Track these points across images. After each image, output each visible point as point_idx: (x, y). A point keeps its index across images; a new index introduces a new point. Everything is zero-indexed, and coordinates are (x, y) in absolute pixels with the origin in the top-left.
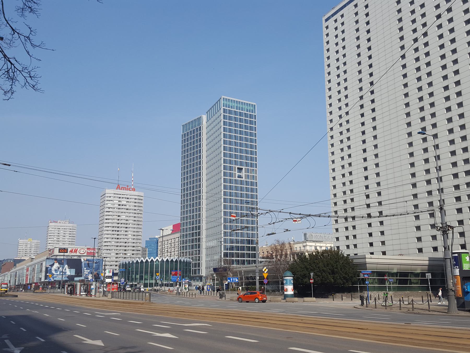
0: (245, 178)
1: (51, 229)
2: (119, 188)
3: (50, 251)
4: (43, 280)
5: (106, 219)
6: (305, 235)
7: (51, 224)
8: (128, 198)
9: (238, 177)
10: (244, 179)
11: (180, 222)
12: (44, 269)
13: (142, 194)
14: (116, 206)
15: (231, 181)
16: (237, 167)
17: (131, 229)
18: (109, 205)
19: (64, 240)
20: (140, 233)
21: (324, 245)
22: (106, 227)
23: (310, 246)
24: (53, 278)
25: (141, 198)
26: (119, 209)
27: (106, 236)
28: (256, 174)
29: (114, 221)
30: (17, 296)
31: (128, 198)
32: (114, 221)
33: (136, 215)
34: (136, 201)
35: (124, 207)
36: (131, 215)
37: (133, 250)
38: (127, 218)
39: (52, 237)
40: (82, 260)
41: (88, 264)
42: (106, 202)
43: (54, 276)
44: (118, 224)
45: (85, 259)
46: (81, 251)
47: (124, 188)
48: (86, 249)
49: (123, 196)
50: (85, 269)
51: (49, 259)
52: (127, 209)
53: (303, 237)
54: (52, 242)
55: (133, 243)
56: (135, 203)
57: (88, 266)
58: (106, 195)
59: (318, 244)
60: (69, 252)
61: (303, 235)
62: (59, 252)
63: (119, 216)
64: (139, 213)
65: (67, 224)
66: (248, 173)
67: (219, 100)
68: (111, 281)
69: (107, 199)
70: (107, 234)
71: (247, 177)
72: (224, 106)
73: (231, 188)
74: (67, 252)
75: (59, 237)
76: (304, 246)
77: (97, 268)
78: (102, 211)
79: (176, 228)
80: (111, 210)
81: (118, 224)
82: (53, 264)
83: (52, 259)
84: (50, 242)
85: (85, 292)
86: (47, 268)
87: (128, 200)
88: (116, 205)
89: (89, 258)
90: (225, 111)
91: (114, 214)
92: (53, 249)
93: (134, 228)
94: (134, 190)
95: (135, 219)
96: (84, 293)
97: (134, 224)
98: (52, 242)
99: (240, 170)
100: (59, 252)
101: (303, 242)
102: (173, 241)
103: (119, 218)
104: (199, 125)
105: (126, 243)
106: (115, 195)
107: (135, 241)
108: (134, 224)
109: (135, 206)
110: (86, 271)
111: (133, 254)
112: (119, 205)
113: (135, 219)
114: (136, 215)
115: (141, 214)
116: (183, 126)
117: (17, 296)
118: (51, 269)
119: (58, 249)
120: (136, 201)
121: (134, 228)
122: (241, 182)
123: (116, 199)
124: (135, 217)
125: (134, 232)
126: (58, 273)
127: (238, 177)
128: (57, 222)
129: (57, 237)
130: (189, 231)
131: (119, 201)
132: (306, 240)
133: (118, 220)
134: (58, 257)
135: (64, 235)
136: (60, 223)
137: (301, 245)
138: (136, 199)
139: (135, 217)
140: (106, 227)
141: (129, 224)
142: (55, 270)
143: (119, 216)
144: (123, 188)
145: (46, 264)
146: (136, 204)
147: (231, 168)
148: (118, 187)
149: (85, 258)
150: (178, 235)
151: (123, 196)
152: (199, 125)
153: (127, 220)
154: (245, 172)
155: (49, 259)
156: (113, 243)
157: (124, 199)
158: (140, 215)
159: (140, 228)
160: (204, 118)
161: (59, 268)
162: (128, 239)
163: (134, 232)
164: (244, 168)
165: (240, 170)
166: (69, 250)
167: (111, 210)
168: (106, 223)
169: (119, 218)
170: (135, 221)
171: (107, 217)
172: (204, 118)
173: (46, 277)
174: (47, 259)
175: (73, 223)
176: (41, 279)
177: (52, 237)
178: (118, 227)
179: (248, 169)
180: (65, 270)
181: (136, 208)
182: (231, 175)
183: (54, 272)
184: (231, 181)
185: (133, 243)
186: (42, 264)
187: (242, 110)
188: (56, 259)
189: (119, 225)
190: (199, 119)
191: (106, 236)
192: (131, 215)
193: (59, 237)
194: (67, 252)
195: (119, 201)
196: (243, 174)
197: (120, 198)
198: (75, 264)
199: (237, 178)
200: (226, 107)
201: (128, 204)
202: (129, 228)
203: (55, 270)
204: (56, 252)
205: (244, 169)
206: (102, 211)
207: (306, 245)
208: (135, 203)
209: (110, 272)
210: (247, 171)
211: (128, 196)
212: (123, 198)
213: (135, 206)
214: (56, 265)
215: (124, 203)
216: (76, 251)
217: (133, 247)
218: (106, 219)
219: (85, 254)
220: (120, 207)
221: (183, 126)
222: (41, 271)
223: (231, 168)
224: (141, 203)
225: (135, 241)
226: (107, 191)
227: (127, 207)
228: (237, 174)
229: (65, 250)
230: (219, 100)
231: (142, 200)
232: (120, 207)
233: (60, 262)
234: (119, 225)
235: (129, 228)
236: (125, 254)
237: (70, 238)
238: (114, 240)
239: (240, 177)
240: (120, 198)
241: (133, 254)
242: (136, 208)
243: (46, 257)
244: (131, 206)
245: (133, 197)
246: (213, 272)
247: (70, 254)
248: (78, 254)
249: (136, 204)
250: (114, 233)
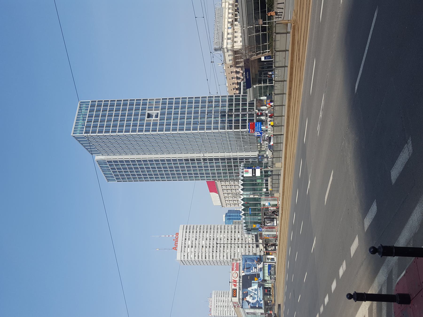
0: (158, 110)
1: (217, 314)
2: (176, 247)
3: (235, 306)
4: (262, 311)
5: (206, 258)
6: (216, 50)
7: (212, 314)
8: (186, 239)
9: (157, 117)
10: (159, 112)
11: (205, 182)
12: (252, 311)
13: (181, 226)
14: (193, 249)
15: (162, 124)
16: (146, 119)
17: (215, 235)
18: (192, 256)
19: (227, 301)
20: (219, 227)
21: (226, 30)
22: (213, 258)
23: (227, 44)
24: (261, 301)
25: (185, 227)
26: (195, 247)
27: (222, 257)
28: (153, 100)
29: (207, 251)
30: (279, 305)
31: (186, 239)
32: (207, 251)
33: (202, 231)
34: (188, 231)
35: (194, 243)
36: (201, 235)
37: (235, 232)
38: (205, 239)
39: (224, 312)
40: (244, 274)
41: (247, 268)
42: (189, 259)
43: (259, 300)
44: (210, 247)
45: (243, 271)
46: (235, 276)
47: (176, 243)
48: (233, 272)
49: (183, 244)
50: (252, 271)
51: (242, 306)
52: (196, 239)
53: (219, 52)
54: (229, 312)
55: (228, 232)
56: (190, 232)
57: (249, 268)
58: (182, 259)
59: (225, 37)
60: (236, 288)
61: (216, 52)
62: (236, 297)
63: (203, 247)
64: (200, 228)
65: (213, 299)
66: (152, 107)
67: (77, 138)
68: (259, 170)
69: (186, 259)
70: (220, 256)
71: (157, 108)
72: (82, 133)
73: (168, 124)
74: (236, 289)
75: (224, 306)
76: (228, 51)
77: (252, 260)
78: (198, 263)
79: (213, 188)
80: (197, 255)
81: (210, 247)
82: (248, 301)
83: (242, 302)
84: (229, 314)
85: (273, 221)
86: (252, 308)
87: (187, 239)
88: (192, 250)
89: (241, 268)
90: (87, 132)
91: (200, 251)
92: (234, 303)
93: (214, 232)
94: (177, 234)
95: (205, 232)
96: (275, 222)
97: (210, 232)
98: (229, 312)
99: (149, 116)
100: (236, 297)
101: (224, 52)
102: (225, 191)
103: (204, 247)
104: (105, 163)
105: (228, 239)
106: (183, 251)
107: (226, 231)
108: (210, 232)
109: (193, 232)
110: (254, 271)
111: (239, 232)
112: (192, 247)
113: (205, 232)
114: (202, 231)
115: (200, 227)
116: (108, 180)
117: (279, 305)
118: (253, 303)
119: (233, 298)
120: (188, 231)
121: (214, 232)
122: (163, 114)
123: (186, 250)
124: (203, 232)
125: (217, 232)
126: (256, 296)
127: (157, 117)
128: (211, 309)
129: (224, 308)
130: (215, 172)
131: (188, 247)
132: (221, 49)
133: (206, 247)
134: (241, 297)
135: (222, 301)
136: (211, 306)
137: (227, 54)
138: (186, 232)
139: (203, 232)
140: (213, 258)
141: (210, 237)
142: (253, 299)
143: (203, 247)
144: (176, 244)
145: (248, 309)
146: (191, 232)
147: (148, 125)
148: (175, 248)
149: (242, 271)
150: (219, 184)
151: (183, 244)
152: (105, 163)
153: (206, 239)
154: (152, 110)
155: (242, 306)
156: (228, 251)
157: (186, 243)
158: (202, 228)
159: (214, 226)
160: (98, 157)
161: (251, 296)
162: (224, 238)
163: (217, 232)
164: (147, 112)
165: (149, 116)
166: (234, 287)
167: (197, 255)
168: (209, 258)
169: (204, 247)
170: (207, 232)
171: (204, 257)
172: (98, 157)
173: (260, 308)
174: (242, 308)
175: (211, 294)
176: (262, 314)
177: (224, 312)
178: (213, 247)
179: (149, 108)
180: (253, 290)
181: (195, 231)
182: (155, 124)
183: (255, 301)
184: (162, 124)
185: (228, 232)
186: (247, 313)
187: (86, 115)
188: (243, 299)
189: (211, 246)
190: (100, 163)
191: (222, 257)
192: (201, 235)
193: (224, 306)
194: (236, 289)
195: (188, 247)
196: (154, 112)
197: (185, 247)
198: (247, 281)
199: (159, 118)
200: (83, 131)
201: (191, 239)
202: (214, 237)
203: (253, 299)
204: (236, 300)
205: (149, 112)
206: (198, 263)
207: (227, 48)
208: (190, 232)
209: (247, 172)
210: (150, 109)
211: (184, 239)
212: (185, 244)
213: (193, 232)
214: (248, 298)
215: (190, 243)
216: (235, 281)
217: (231, 232)
218: (206, 258)
219: (238, 272)
220: (194, 246)
221: (108, 180)
222: (254, 314)
223: (148, 125)
224: (190, 226)
225: (226, 231)
226: (178, 258)
227: (194, 239)
228: (154, 118)
229: (234, 291)
230: (77, 138)
231: (187, 227)
232: (194, 246)
233: (245, 295)
234: (211, 246)
235: (214, 237)
236: (238, 239)
237: (225, 296)
238: (225, 250)
239: (157, 116)
240: (185, 247)
241: (239, 232)
242: (195, 231)
243: (241, 309)
244: (192, 236)
245: (184, 235)
246: (251, 89)
247: (238, 286)
248: (237, 279)
249: (191, 232)
250: (218, 250)
